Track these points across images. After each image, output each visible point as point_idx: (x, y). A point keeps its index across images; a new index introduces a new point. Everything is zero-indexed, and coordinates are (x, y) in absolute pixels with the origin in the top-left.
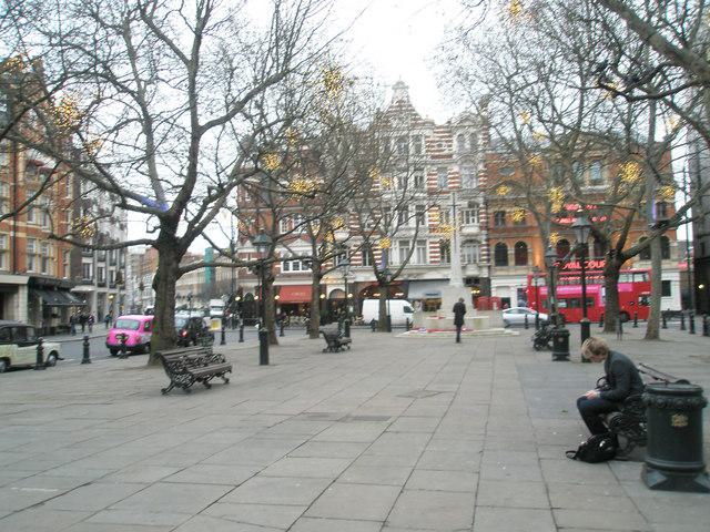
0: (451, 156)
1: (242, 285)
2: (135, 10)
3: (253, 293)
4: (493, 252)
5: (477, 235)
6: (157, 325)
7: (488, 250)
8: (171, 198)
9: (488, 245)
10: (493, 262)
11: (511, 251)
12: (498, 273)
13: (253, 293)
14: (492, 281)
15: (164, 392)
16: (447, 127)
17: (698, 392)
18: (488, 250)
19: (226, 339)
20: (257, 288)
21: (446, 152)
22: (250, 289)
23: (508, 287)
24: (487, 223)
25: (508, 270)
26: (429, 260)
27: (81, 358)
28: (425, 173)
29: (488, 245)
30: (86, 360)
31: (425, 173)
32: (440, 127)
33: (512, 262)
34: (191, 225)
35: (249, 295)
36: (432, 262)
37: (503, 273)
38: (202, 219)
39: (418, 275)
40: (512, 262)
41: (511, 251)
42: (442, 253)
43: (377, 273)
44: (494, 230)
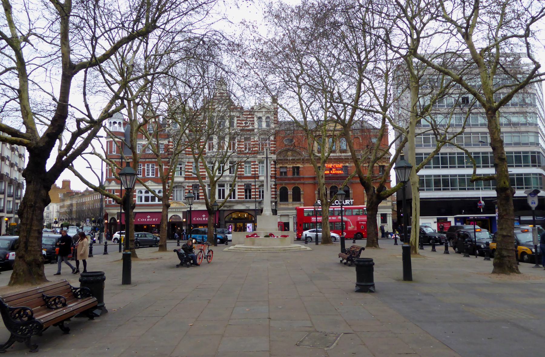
0: (253, 130)
1: (107, 211)
2: (159, 27)
3: (116, 217)
4: (278, 193)
5: (182, 183)
6: (22, 245)
7: (276, 191)
8: (41, 130)
9: (275, 188)
10: (278, 199)
11: (290, 192)
12: (282, 206)
13: (116, 217)
14: (278, 212)
15: (178, 266)
16: (250, 112)
17: (371, 260)
18: (276, 191)
19: (93, 252)
20: (119, 215)
21: (251, 127)
22: (114, 214)
23: (288, 215)
24: (275, 174)
25: (288, 205)
26: (237, 197)
27: (103, 251)
28: (236, 140)
29: (275, 188)
30: (106, 252)
31: (236, 140)
32: (247, 111)
33: (290, 200)
34: (60, 157)
35: (113, 218)
36: (238, 198)
37: (284, 206)
38: (70, 153)
39: (230, 206)
40: (290, 200)
41: (290, 192)
42: (246, 192)
43: (207, 204)
44: (280, 179)
